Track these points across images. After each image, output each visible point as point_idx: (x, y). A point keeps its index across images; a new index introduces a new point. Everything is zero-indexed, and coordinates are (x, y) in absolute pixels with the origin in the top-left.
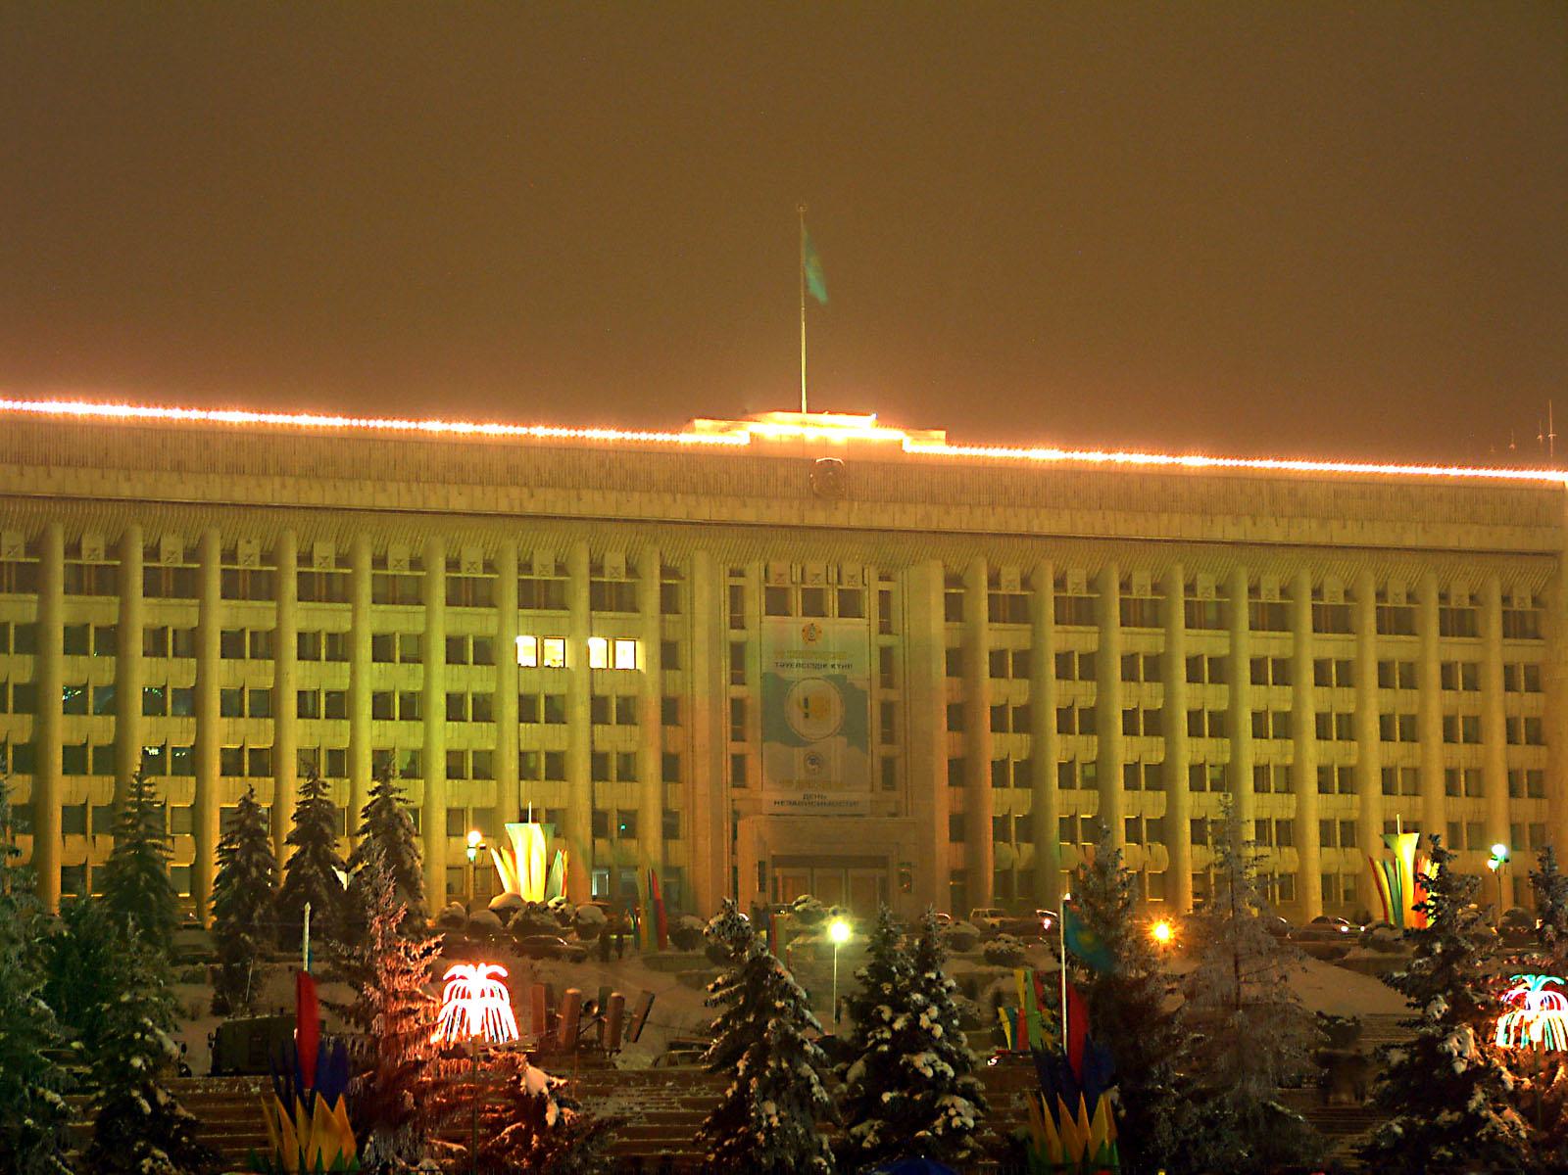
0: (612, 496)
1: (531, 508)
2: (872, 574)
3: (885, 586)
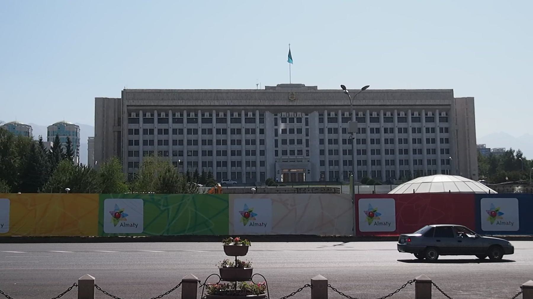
0: (248, 101)
1: (231, 104)
2: (304, 114)
3: (306, 117)
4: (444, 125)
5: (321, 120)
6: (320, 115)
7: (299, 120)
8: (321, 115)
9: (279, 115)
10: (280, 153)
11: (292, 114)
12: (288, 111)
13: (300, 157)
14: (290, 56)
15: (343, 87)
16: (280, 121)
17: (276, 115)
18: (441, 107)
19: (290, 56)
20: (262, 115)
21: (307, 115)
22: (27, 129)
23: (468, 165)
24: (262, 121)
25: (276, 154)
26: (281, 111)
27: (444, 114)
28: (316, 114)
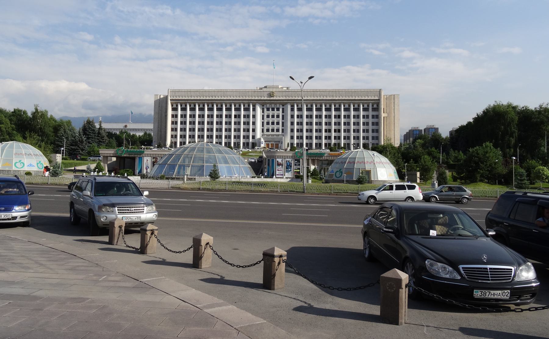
2: (281, 106)
4: (375, 113)
5: (292, 110)
6: (291, 106)
7: (278, 109)
8: (292, 106)
9: (265, 106)
10: (265, 130)
11: (273, 106)
12: (271, 104)
13: (278, 133)
14: (293, 79)
15: (288, 88)
16: (265, 110)
17: (263, 106)
18: (373, 101)
19: (293, 79)
20: (254, 107)
21: (283, 106)
22: (25, 112)
23: (253, 188)
24: (254, 110)
25: (263, 131)
26: (266, 104)
27: (375, 106)
28: (289, 107)
